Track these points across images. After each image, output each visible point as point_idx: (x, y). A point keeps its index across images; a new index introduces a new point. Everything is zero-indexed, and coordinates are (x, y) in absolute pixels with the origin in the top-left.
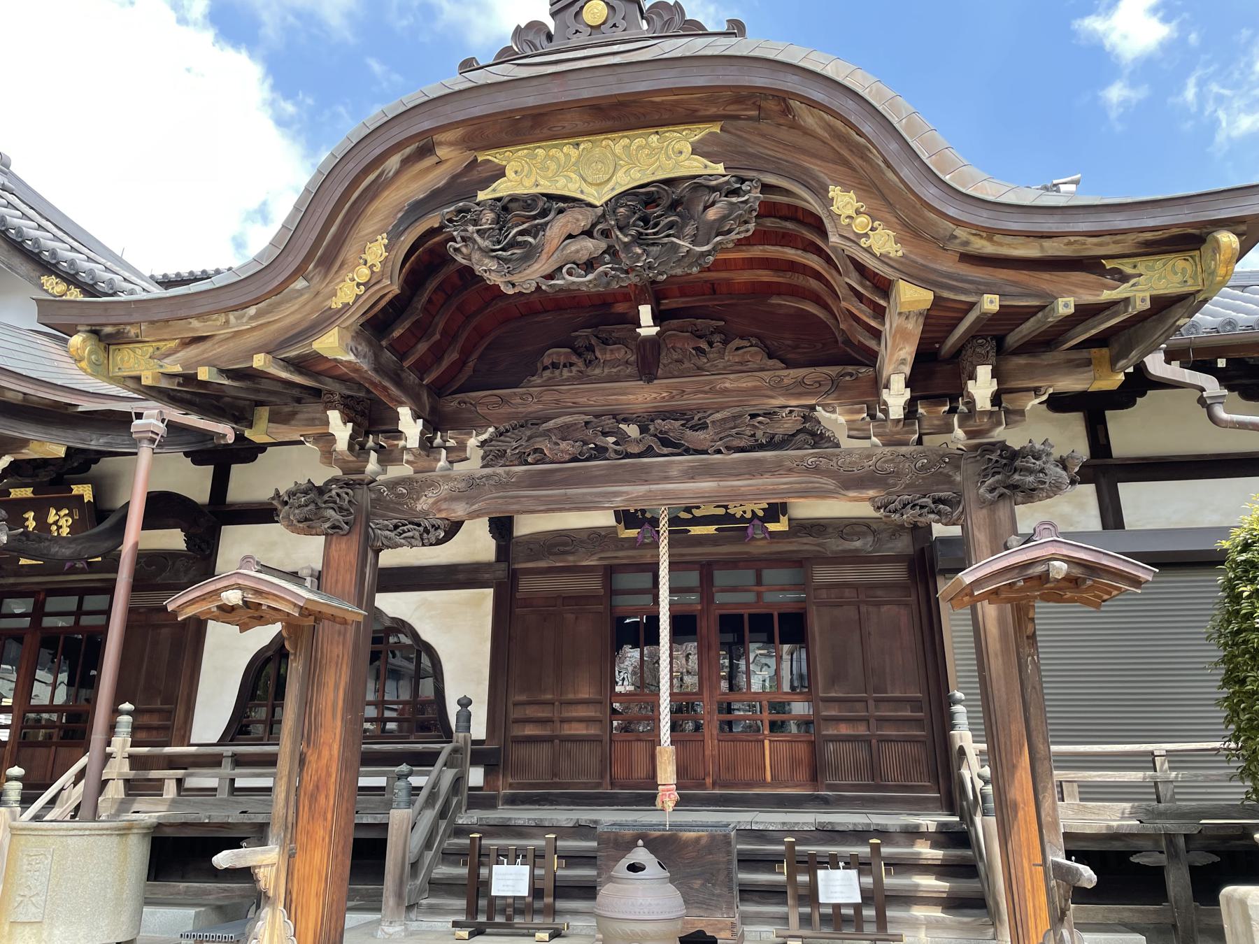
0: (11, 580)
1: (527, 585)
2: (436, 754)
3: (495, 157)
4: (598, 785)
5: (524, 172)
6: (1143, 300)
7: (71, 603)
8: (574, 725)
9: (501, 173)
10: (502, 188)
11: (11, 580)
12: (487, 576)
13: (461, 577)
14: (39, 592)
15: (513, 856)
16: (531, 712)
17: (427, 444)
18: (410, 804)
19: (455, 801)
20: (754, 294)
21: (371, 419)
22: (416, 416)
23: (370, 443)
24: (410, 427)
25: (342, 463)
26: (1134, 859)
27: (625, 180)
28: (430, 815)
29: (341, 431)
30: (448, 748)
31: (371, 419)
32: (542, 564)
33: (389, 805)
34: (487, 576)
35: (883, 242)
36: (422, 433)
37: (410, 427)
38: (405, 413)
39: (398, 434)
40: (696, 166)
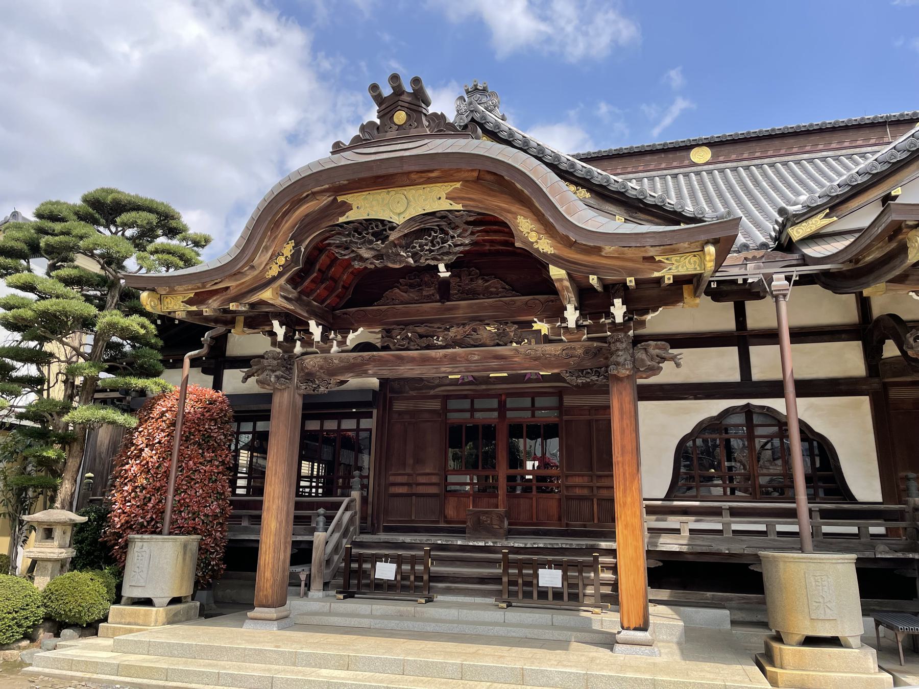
0: (484, 387)
1: (894, 393)
2: (341, 503)
3: (348, 198)
4: (438, 522)
5: (365, 207)
6: (669, 279)
7: (466, 404)
8: (420, 487)
9: (349, 208)
10: (352, 216)
11: (484, 387)
12: (864, 387)
13: (843, 387)
14: (501, 395)
15: (386, 558)
16: (399, 479)
17: (325, 338)
18: (326, 530)
19: (352, 529)
20: (496, 266)
21: (295, 324)
22: (281, 325)
23: (297, 336)
24: (316, 331)
25: (280, 345)
26: (751, 568)
27: (416, 210)
28: (337, 536)
29: (280, 331)
30: (346, 500)
31: (295, 324)
32: (909, 379)
33: (312, 531)
34: (864, 387)
35: (545, 246)
36: (322, 333)
37: (316, 331)
38: (312, 323)
39: (564, 320)
40: (445, 205)
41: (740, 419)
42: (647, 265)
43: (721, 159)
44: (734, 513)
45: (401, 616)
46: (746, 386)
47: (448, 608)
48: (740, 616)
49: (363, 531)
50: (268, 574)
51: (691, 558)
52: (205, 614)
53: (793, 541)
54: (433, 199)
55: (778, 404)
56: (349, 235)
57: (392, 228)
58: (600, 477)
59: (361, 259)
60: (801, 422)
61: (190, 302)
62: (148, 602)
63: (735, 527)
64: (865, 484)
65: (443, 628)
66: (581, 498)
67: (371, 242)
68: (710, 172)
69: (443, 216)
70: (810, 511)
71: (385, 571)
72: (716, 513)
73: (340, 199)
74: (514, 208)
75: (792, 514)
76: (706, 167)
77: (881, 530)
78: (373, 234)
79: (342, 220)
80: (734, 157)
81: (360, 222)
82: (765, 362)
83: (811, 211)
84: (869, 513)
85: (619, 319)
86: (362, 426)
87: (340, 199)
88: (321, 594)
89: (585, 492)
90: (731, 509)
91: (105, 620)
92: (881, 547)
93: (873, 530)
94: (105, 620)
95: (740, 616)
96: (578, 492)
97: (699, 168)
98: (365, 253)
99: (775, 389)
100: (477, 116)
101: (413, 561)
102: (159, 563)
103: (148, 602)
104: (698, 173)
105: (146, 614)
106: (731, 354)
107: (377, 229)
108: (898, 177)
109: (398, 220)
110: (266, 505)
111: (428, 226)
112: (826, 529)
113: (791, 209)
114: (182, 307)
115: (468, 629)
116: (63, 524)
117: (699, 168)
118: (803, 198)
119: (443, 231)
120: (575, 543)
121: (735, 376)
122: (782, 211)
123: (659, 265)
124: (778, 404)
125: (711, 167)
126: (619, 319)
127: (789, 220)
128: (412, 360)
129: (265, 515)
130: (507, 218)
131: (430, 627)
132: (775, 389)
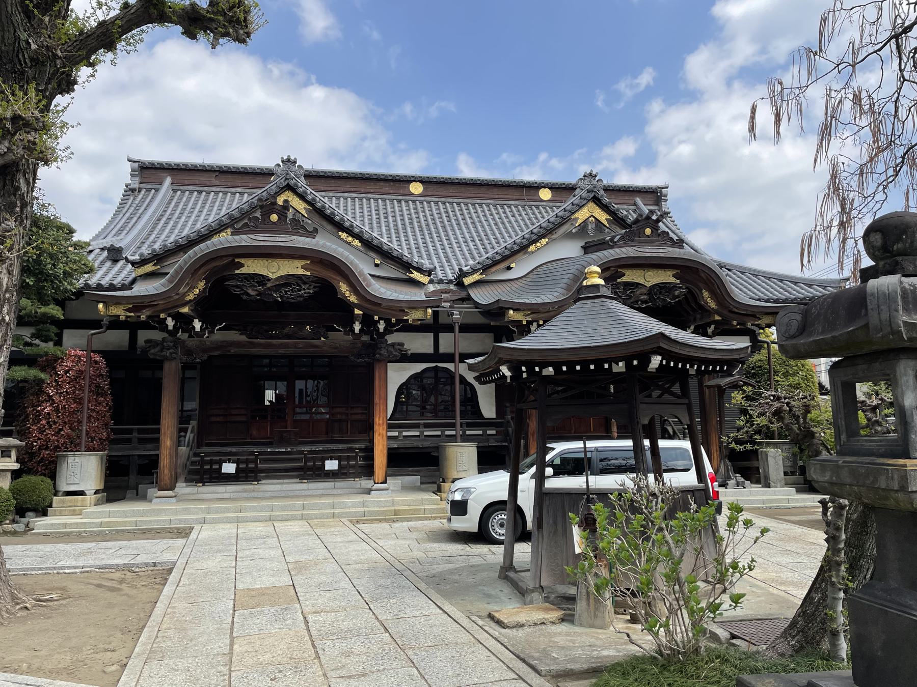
2: (187, 428)
3: (242, 261)
9: (242, 265)
10: (244, 270)
35: (353, 299)
37: (197, 325)
40: (301, 272)
41: (432, 374)
42: (401, 313)
43: (430, 193)
44: (427, 426)
45: (249, 491)
46: (436, 356)
47: (270, 486)
48: (425, 480)
49: (198, 447)
50: (166, 471)
51: (402, 451)
52: (110, 500)
53: (453, 439)
54: (295, 268)
55: (450, 366)
56: (242, 281)
57: (269, 280)
58: (352, 408)
59: (248, 294)
60: (460, 375)
61: (129, 310)
62: (81, 493)
63: (426, 433)
64: (488, 409)
65: (276, 494)
66: (340, 421)
67: (255, 286)
68: (421, 202)
69: (299, 277)
70: (461, 424)
71: (229, 468)
72: (416, 426)
73: (237, 260)
74: (338, 278)
75: (452, 426)
76: (419, 198)
77: (494, 432)
78: (257, 282)
79: (237, 272)
80: (435, 193)
81: (249, 274)
82: (447, 342)
83: (474, 271)
84: (489, 424)
85: (381, 330)
86: (587, 445)
87: (237, 260)
88: (184, 484)
89: (344, 417)
90: (138, 429)
91: (51, 506)
92: (492, 440)
93: (489, 432)
94: (51, 506)
95: (425, 480)
96: (339, 417)
97: (415, 198)
98: (250, 291)
99: (449, 358)
100: (292, 182)
101: (247, 462)
102: (84, 470)
103: (81, 493)
104: (414, 202)
105: (83, 500)
106: (430, 336)
107: (262, 280)
108: (514, 258)
109: (271, 276)
110: (162, 431)
111: (288, 281)
112: (468, 433)
113: (465, 269)
114: (123, 313)
115: (291, 494)
116: (14, 447)
117: (415, 198)
118: (471, 262)
119: (299, 285)
120: (345, 446)
121: (431, 350)
122: (460, 270)
123: (407, 314)
124: (450, 366)
125: (422, 199)
126: (381, 330)
127: (462, 274)
128: (260, 345)
129: (162, 437)
130: (334, 283)
131: (267, 495)
132: (449, 358)
